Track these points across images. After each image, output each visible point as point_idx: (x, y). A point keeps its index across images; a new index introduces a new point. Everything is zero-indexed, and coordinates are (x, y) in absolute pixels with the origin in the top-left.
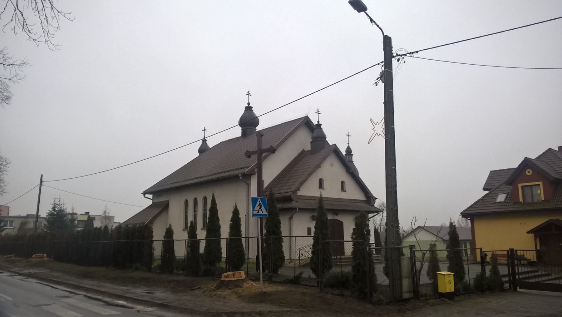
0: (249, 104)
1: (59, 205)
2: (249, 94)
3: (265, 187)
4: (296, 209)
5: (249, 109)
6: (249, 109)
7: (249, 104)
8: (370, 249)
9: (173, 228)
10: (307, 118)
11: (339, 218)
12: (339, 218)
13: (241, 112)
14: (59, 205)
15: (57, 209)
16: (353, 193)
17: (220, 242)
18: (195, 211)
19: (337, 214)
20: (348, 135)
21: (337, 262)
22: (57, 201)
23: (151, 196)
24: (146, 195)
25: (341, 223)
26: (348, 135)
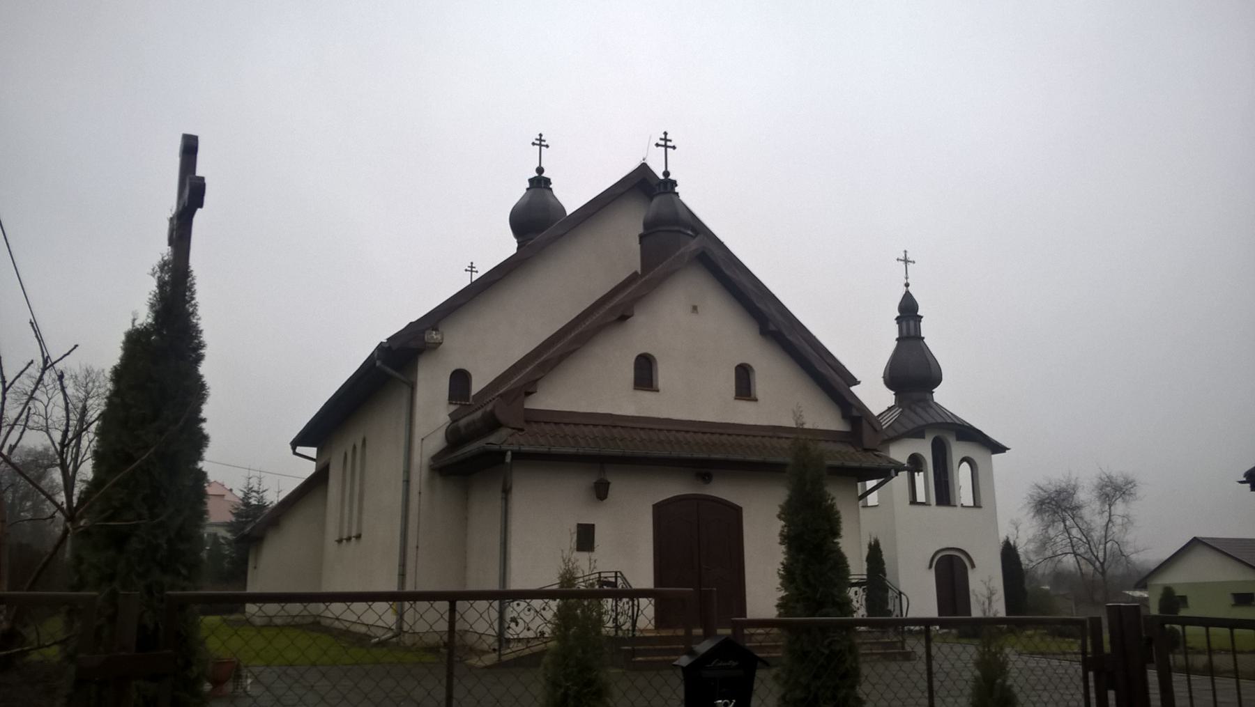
0: (540, 170)
1: (258, 492)
2: (540, 142)
3: (473, 393)
4: (503, 453)
5: (540, 183)
6: (540, 183)
7: (540, 170)
8: (600, 614)
9: (882, 547)
10: (643, 170)
11: (722, 490)
12: (722, 490)
13: (517, 191)
14: (258, 492)
15: (253, 501)
16: (783, 403)
17: (659, 579)
18: (352, 488)
19: (706, 478)
20: (906, 261)
21: (634, 653)
22: (254, 484)
23: (312, 451)
24: (300, 449)
25: (738, 511)
26: (906, 261)
